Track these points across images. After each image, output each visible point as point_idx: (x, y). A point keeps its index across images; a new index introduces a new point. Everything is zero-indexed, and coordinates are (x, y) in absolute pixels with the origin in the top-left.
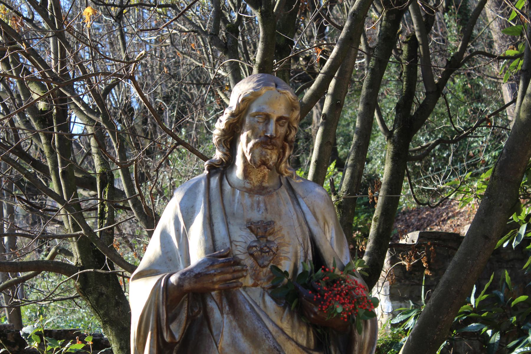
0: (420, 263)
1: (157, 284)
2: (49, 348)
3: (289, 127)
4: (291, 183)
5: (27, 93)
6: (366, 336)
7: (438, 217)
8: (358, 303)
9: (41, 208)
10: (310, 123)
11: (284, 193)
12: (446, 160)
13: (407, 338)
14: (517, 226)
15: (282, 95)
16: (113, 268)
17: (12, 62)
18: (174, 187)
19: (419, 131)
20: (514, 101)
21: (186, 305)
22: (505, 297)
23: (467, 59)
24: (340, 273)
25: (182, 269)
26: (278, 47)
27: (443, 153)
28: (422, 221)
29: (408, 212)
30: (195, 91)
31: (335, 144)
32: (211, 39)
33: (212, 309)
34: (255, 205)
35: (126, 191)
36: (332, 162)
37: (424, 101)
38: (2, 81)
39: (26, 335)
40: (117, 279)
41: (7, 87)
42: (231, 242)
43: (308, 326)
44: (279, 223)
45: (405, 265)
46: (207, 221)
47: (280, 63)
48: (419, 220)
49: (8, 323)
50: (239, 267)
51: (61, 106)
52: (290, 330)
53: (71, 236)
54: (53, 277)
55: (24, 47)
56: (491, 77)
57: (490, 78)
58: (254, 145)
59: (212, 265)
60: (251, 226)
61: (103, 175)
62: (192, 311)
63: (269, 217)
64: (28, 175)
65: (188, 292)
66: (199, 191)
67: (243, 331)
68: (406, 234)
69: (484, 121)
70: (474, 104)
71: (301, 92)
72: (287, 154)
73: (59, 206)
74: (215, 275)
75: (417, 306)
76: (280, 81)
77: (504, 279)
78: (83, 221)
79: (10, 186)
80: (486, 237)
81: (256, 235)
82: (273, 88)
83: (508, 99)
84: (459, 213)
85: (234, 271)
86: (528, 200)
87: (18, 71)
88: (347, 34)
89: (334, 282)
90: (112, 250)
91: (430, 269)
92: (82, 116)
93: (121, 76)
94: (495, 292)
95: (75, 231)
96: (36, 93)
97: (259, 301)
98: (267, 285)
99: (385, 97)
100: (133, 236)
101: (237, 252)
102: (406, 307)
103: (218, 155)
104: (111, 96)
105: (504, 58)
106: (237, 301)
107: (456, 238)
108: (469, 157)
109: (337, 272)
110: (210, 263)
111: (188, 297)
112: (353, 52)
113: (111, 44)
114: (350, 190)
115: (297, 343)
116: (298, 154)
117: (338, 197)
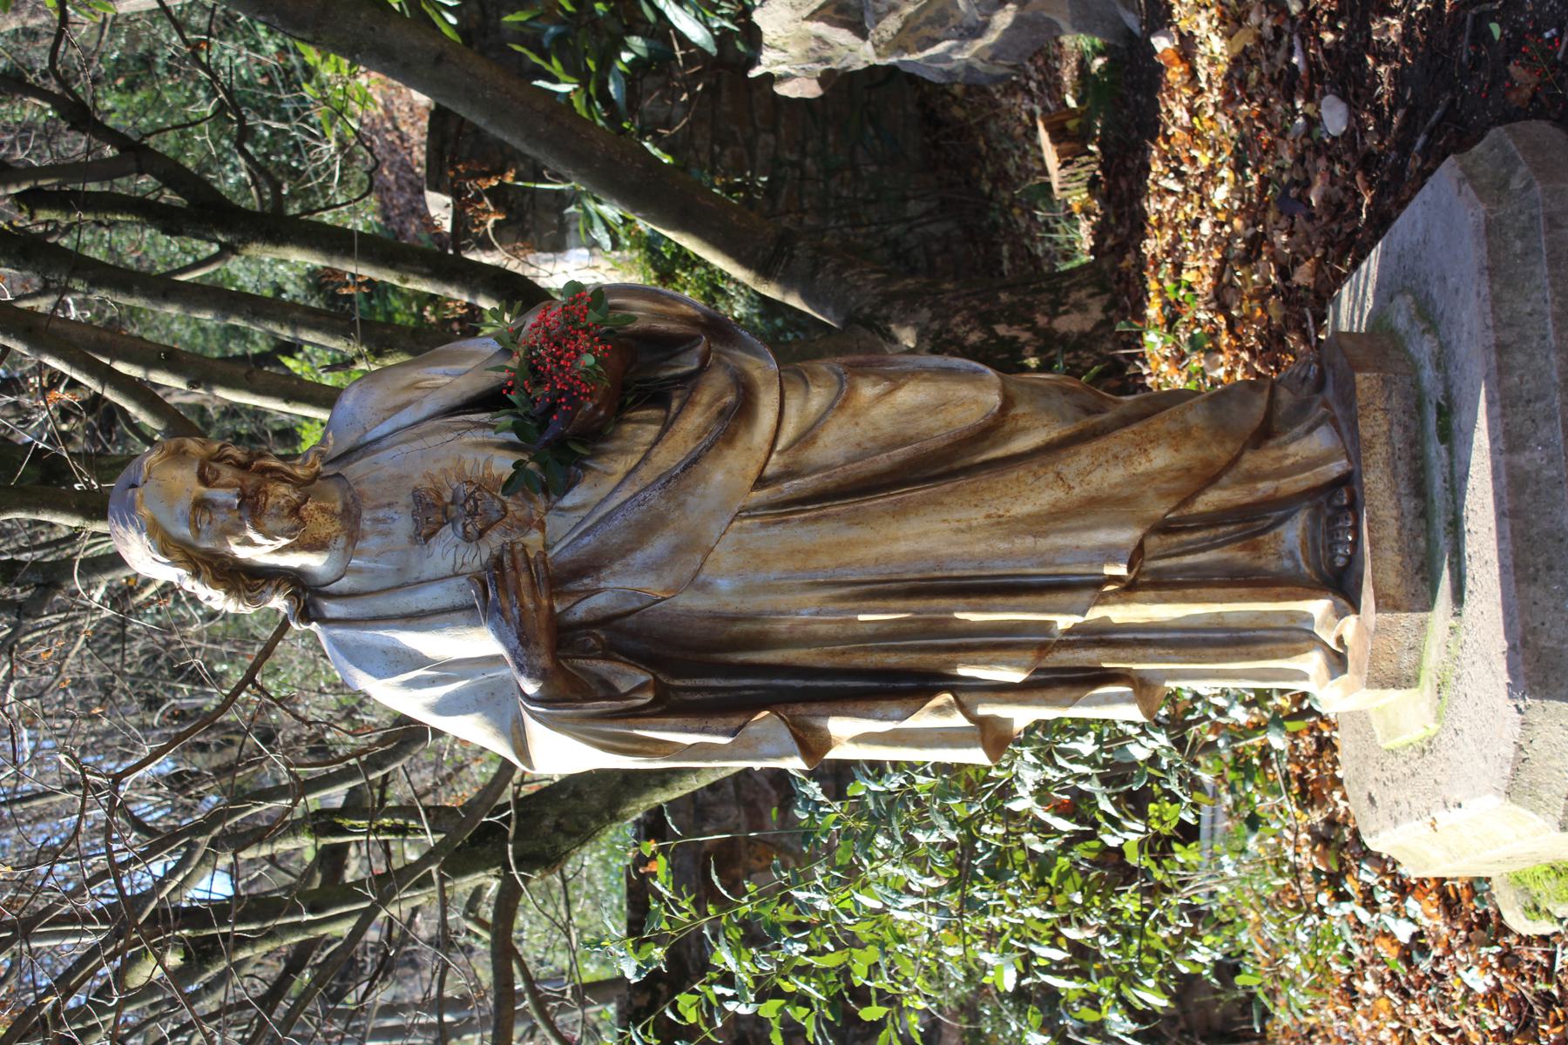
0: (491, 192)
1: (540, 721)
2: (665, 926)
3: (219, 460)
4: (335, 455)
5: (151, 988)
6: (639, 306)
7: (395, 151)
8: (575, 322)
9: (387, 952)
10: (201, 410)
11: (356, 470)
12: (274, 132)
13: (639, 221)
15: (154, 475)
16: (506, 806)
17: (82, 1022)
18: (337, 686)
19: (216, 185)
21: (582, 663)
22: (556, 24)
23: (64, 83)
24: (517, 359)
25: (511, 670)
26: (45, 481)
27: (263, 137)
28: (403, 182)
29: (384, 211)
30: (138, 645)
31: (244, 358)
32: (28, 616)
33: (590, 611)
34: (381, 527)
35: (351, 784)
36: (282, 365)
37: (157, 177)
38: (123, 1040)
39: (639, 970)
40: (528, 797)
41: (135, 1030)
42: (456, 575)
43: (621, 421)
44: (418, 480)
45: (497, 222)
46: (415, 623)
47: (81, 474)
48: (401, 188)
49: (614, 1005)
50: (506, 559)
51: (176, 919)
52: (629, 458)
53: (442, 890)
54: (521, 919)
55: (51, 1000)
56: (102, 34)
57: (104, 38)
58: (259, 532)
59: (502, 612)
60: (424, 534)
61: (317, 832)
62: (593, 649)
63: (405, 499)
64: (317, 981)
65: (555, 658)
66: (354, 640)
67: (632, 550)
68: (432, 219)
70: (159, 71)
72: (275, 463)
73: (383, 914)
74: (522, 606)
75: (575, 198)
77: (521, 23)
78: (411, 868)
79: (340, 1014)
80: (439, 59)
81: (442, 524)
82: (138, 493)
84: (385, 108)
85: (514, 568)
87: (102, 1010)
88: (18, 338)
89: (533, 370)
90: (469, 807)
91: (501, 172)
92: (195, 877)
93: (112, 800)
94: (546, 42)
95: (431, 883)
96: (145, 972)
97: (574, 518)
98: (541, 502)
99: (146, 253)
100: (438, 765)
101: (477, 562)
102: (577, 220)
103: (279, 603)
104: (148, 818)
106: (573, 561)
107: (439, 117)
108: (271, 85)
109: (514, 362)
110: (498, 616)
111: (565, 658)
112: (57, 325)
113: (38, 819)
114: (345, 333)
115: (655, 444)
116: (265, 433)
117: (360, 356)
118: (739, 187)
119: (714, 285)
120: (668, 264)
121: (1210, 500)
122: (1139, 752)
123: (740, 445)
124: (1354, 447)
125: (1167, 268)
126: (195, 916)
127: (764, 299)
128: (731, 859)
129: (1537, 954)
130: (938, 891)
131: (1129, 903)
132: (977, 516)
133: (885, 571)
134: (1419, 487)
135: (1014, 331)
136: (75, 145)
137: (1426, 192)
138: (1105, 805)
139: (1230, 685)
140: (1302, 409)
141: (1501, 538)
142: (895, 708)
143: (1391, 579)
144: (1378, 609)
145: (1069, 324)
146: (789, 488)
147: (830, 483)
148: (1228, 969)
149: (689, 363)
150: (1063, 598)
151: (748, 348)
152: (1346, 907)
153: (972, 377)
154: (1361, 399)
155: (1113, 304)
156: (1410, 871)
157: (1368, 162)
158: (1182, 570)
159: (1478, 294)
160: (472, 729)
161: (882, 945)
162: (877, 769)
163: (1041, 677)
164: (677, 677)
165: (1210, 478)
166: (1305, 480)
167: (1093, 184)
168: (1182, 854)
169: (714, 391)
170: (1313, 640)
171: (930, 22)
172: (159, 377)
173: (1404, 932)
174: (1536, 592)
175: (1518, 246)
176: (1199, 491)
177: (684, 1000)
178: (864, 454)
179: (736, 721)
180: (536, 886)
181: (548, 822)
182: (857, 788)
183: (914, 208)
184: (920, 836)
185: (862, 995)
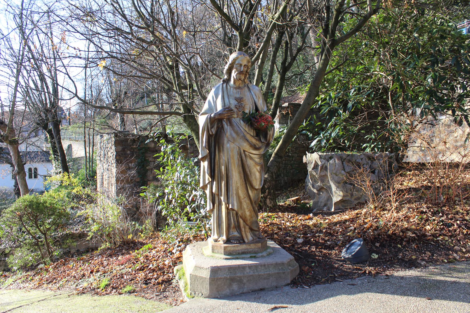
0: (288, 112)
5: (166, 60)
10: (254, 69)
11: (246, 89)
14: (318, 101)
20: (318, 62)
25: (215, 112)
43: (254, 129)
60: (236, 99)
65: (217, 119)
69: (308, 68)
71: (251, 59)
73: (177, 94)
75: (287, 126)
76: (245, 53)
80: (309, 104)
83: (316, 61)
90: (193, 108)
97: (239, 122)
98: (241, 117)
103: (226, 77)
105: (315, 48)
108: (304, 80)
109: (263, 113)
118: (289, 151)
119: (274, 147)
120: (277, 140)
121: (241, 221)
122: (202, 211)
123: (250, 148)
124: (249, 243)
125: (277, 216)
126: (177, 66)
127: (272, 155)
128: (184, 148)
129: (171, 271)
130: (180, 180)
131: (178, 210)
132: (239, 185)
133: (230, 170)
134: (243, 253)
135: (267, 193)
136: (295, 52)
137: (289, 254)
138: (193, 205)
139: (212, 225)
140: (255, 235)
141: (235, 265)
142: (209, 172)
143: (229, 249)
144: (224, 247)
145: (268, 201)
146: (243, 155)
147: (244, 162)
148: (168, 224)
149: (263, 140)
150: (226, 198)
151: (265, 149)
152: (178, 243)
153: (260, 184)
154: (257, 244)
155: (271, 208)
156: (183, 252)
157: (293, 246)
158: (230, 216)
160: (206, 107)
161: (172, 171)
162: (199, 170)
165: (245, 221)
166: (244, 236)
167: (290, 205)
168: (186, 218)
169: (258, 144)
170: (219, 237)
171: (315, 179)
172: (260, 61)
173: (174, 251)
174: (227, 270)
175: (280, 268)
176: (243, 219)
177: (164, 140)
178: (249, 167)
179: (207, 147)
180: (180, 118)
181: (191, 120)
182: (196, 168)
183: (286, 178)
184: (189, 176)
185: (164, 168)
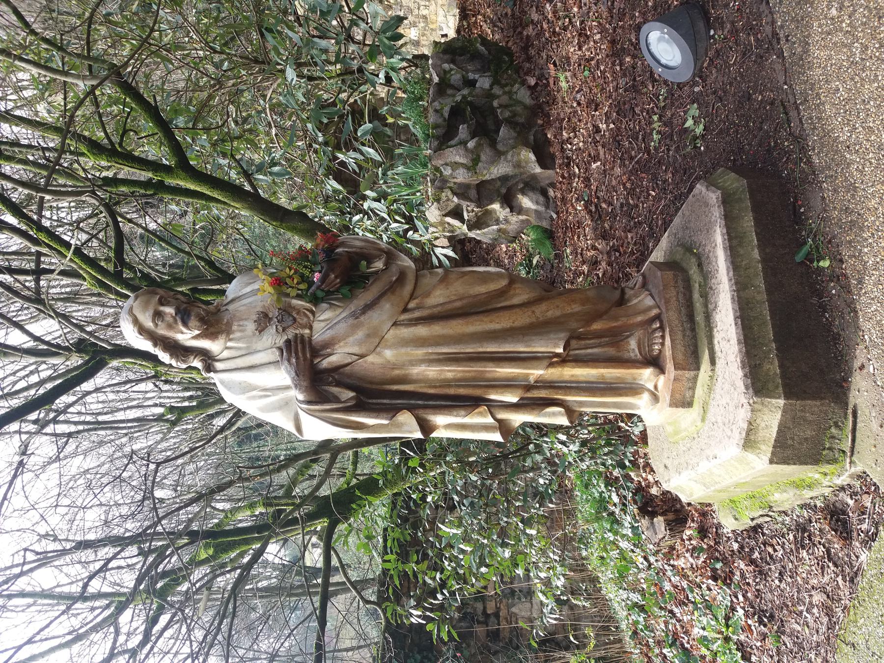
33: (329, 363)
60: (261, 329)
67: (348, 336)
86: (763, 7)
143: (680, 357)
146: (417, 314)
150: (535, 363)
158: (586, 355)
159: (563, 443)
163: (525, 402)
164: (370, 399)
165: (598, 316)
